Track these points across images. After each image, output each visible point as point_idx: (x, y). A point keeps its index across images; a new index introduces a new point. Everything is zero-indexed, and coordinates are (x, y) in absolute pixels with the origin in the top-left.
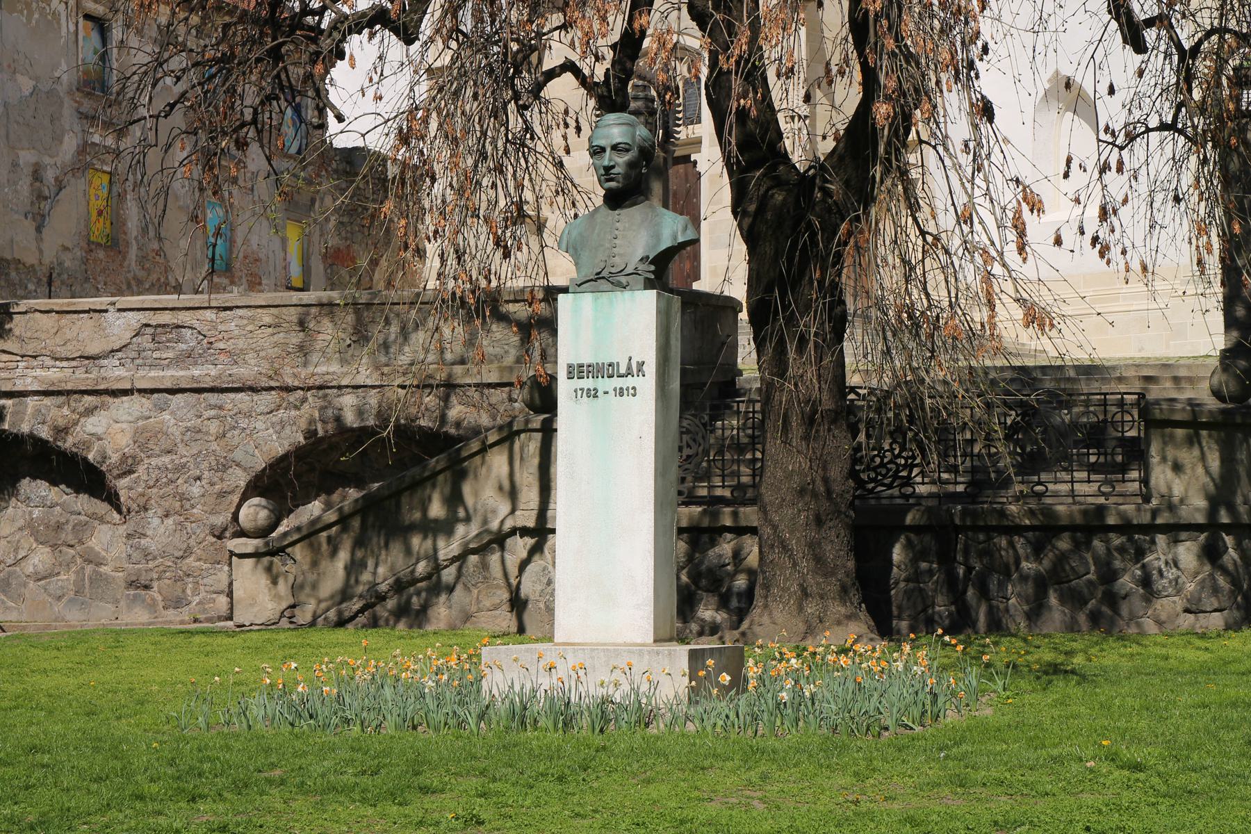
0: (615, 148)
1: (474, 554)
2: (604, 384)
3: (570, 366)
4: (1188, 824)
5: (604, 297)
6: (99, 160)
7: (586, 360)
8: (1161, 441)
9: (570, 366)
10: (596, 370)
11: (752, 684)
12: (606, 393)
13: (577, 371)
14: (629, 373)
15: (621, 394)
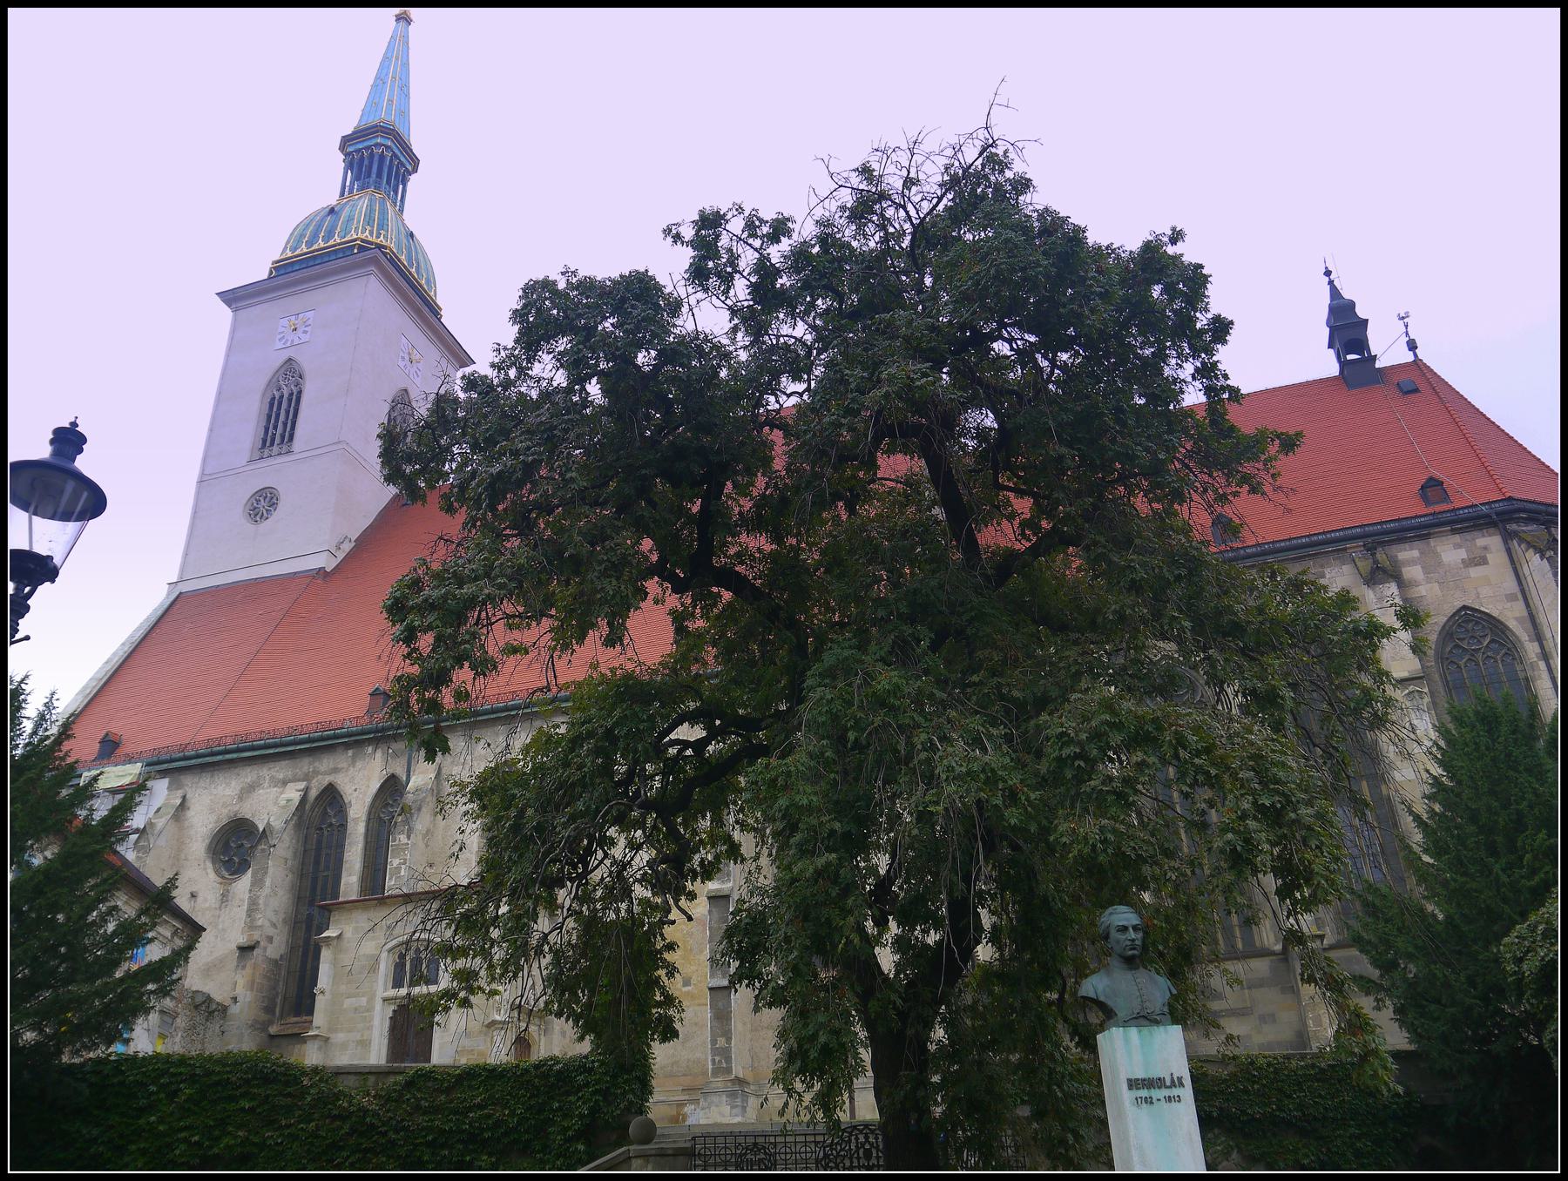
0: (1135, 928)
2: (1157, 1094)
3: (1129, 1081)
5: (1145, 1030)
7: (1140, 1074)
8: (365, 723)
9: (1129, 1081)
10: (1149, 1083)
11: (784, 762)
12: (1159, 1100)
13: (1133, 1084)
14: (1173, 1085)
15: (1170, 1100)
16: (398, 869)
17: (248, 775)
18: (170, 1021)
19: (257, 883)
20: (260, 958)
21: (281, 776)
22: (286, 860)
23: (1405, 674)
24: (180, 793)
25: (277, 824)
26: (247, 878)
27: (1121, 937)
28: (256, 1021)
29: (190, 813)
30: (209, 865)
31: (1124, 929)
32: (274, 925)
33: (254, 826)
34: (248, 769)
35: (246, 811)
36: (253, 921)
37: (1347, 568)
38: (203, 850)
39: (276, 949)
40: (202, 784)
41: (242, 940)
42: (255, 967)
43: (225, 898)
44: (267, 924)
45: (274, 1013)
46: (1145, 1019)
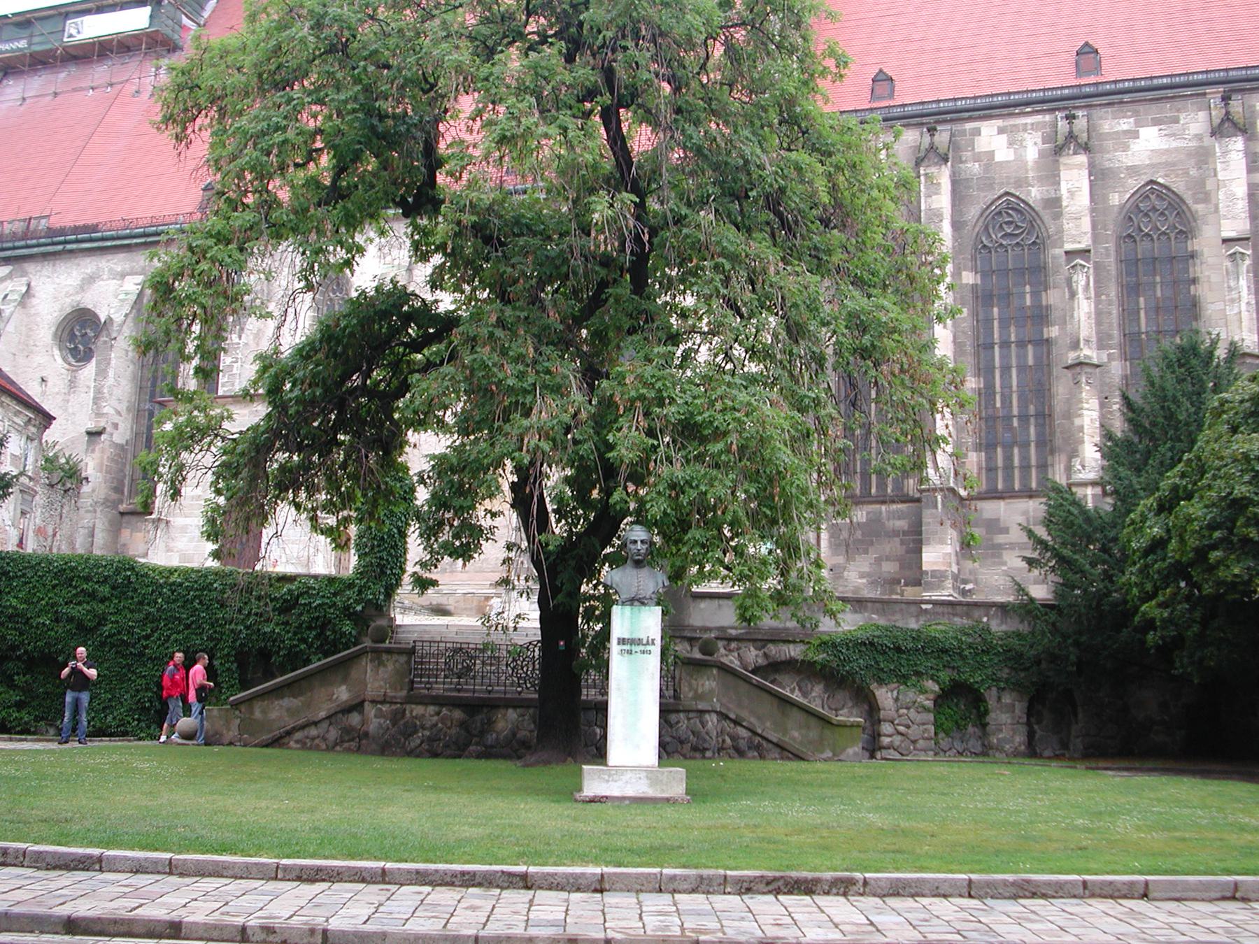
0: (642, 542)
1: (515, 707)
2: (635, 648)
4: (866, 340)
5: (636, 609)
6: (375, 500)
7: (626, 636)
10: (633, 642)
13: (622, 641)
14: (648, 643)
16: (231, 367)
17: (89, 265)
18: (30, 498)
19: (101, 373)
20: (107, 443)
21: (119, 269)
22: (127, 351)
23: (1233, 234)
24: (24, 280)
25: (118, 318)
26: (93, 364)
27: (632, 547)
28: (106, 500)
29: (34, 301)
30: (57, 352)
31: (635, 542)
32: (119, 413)
33: (95, 315)
34: (88, 260)
35: (88, 301)
36: (99, 408)
37: (1202, 115)
38: (50, 337)
39: (122, 434)
40: (45, 272)
41: (91, 426)
42: (103, 451)
43: (72, 384)
44: (112, 411)
45: (122, 493)
46: (637, 601)
